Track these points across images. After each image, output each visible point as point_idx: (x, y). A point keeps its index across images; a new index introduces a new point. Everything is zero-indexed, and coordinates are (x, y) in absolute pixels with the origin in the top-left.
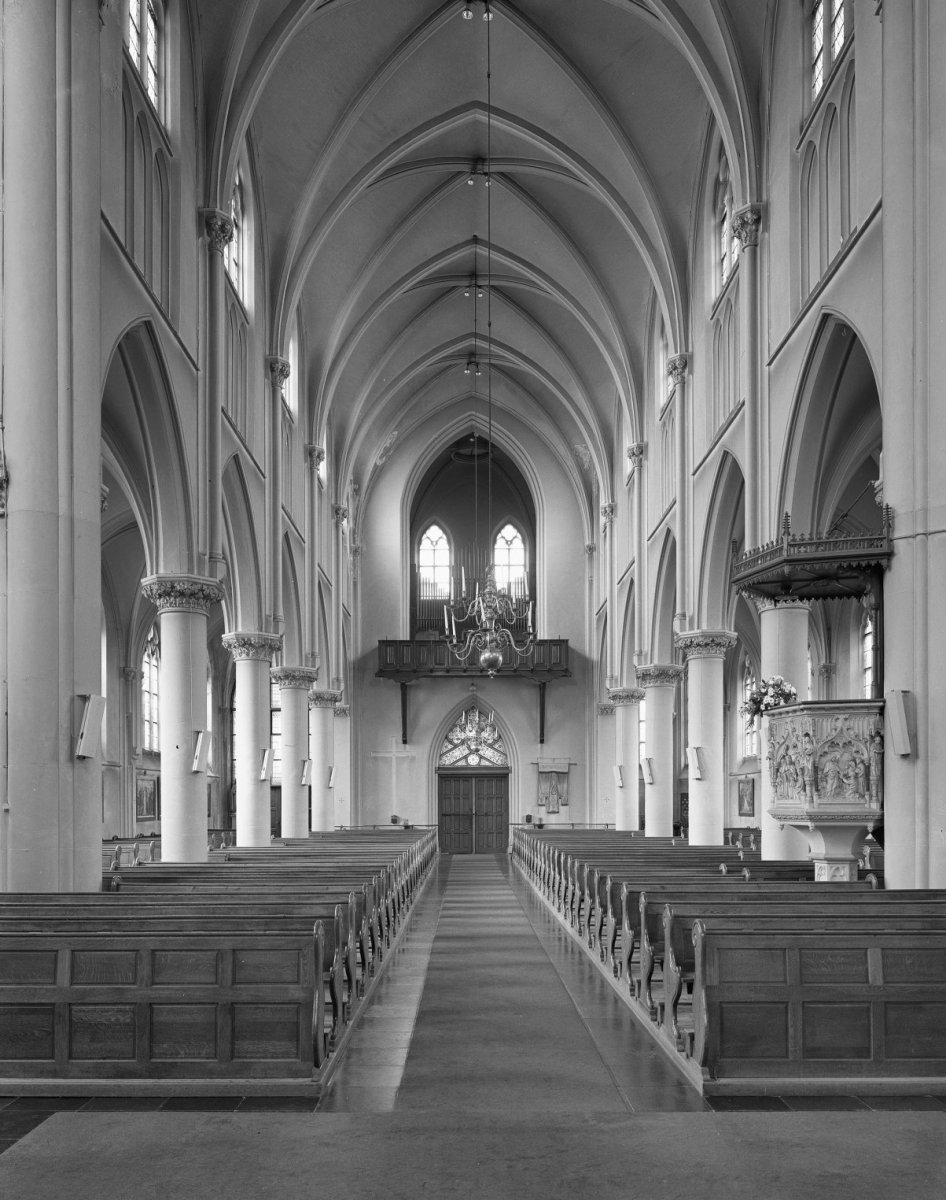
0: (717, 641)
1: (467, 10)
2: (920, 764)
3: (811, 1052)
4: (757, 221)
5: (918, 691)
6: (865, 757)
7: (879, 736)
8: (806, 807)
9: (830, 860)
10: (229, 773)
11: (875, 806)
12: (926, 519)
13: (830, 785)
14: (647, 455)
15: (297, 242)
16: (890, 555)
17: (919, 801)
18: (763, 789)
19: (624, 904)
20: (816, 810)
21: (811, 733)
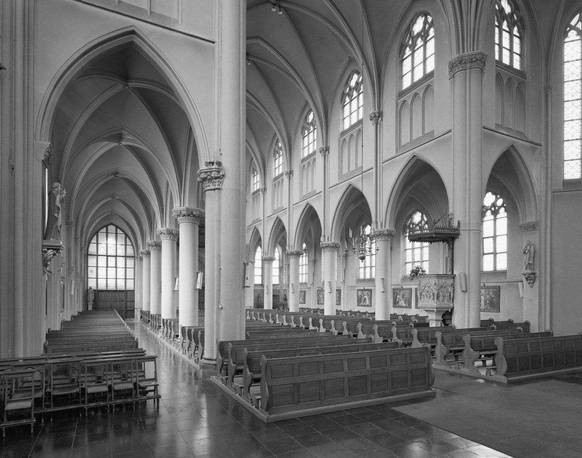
0: (337, 246)
1: (273, 8)
2: (467, 293)
3: (521, 369)
4: (379, 117)
5: (467, 273)
6: (450, 290)
7: (453, 285)
8: (435, 305)
9: (436, 320)
10: (86, 284)
11: (452, 305)
12: (469, 225)
13: (441, 299)
14: (293, 174)
15: (527, 181)
16: (459, 234)
17: (467, 303)
18: (377, 295)
19: (192, 336)
20: (438, 306)
21: (437, 283)
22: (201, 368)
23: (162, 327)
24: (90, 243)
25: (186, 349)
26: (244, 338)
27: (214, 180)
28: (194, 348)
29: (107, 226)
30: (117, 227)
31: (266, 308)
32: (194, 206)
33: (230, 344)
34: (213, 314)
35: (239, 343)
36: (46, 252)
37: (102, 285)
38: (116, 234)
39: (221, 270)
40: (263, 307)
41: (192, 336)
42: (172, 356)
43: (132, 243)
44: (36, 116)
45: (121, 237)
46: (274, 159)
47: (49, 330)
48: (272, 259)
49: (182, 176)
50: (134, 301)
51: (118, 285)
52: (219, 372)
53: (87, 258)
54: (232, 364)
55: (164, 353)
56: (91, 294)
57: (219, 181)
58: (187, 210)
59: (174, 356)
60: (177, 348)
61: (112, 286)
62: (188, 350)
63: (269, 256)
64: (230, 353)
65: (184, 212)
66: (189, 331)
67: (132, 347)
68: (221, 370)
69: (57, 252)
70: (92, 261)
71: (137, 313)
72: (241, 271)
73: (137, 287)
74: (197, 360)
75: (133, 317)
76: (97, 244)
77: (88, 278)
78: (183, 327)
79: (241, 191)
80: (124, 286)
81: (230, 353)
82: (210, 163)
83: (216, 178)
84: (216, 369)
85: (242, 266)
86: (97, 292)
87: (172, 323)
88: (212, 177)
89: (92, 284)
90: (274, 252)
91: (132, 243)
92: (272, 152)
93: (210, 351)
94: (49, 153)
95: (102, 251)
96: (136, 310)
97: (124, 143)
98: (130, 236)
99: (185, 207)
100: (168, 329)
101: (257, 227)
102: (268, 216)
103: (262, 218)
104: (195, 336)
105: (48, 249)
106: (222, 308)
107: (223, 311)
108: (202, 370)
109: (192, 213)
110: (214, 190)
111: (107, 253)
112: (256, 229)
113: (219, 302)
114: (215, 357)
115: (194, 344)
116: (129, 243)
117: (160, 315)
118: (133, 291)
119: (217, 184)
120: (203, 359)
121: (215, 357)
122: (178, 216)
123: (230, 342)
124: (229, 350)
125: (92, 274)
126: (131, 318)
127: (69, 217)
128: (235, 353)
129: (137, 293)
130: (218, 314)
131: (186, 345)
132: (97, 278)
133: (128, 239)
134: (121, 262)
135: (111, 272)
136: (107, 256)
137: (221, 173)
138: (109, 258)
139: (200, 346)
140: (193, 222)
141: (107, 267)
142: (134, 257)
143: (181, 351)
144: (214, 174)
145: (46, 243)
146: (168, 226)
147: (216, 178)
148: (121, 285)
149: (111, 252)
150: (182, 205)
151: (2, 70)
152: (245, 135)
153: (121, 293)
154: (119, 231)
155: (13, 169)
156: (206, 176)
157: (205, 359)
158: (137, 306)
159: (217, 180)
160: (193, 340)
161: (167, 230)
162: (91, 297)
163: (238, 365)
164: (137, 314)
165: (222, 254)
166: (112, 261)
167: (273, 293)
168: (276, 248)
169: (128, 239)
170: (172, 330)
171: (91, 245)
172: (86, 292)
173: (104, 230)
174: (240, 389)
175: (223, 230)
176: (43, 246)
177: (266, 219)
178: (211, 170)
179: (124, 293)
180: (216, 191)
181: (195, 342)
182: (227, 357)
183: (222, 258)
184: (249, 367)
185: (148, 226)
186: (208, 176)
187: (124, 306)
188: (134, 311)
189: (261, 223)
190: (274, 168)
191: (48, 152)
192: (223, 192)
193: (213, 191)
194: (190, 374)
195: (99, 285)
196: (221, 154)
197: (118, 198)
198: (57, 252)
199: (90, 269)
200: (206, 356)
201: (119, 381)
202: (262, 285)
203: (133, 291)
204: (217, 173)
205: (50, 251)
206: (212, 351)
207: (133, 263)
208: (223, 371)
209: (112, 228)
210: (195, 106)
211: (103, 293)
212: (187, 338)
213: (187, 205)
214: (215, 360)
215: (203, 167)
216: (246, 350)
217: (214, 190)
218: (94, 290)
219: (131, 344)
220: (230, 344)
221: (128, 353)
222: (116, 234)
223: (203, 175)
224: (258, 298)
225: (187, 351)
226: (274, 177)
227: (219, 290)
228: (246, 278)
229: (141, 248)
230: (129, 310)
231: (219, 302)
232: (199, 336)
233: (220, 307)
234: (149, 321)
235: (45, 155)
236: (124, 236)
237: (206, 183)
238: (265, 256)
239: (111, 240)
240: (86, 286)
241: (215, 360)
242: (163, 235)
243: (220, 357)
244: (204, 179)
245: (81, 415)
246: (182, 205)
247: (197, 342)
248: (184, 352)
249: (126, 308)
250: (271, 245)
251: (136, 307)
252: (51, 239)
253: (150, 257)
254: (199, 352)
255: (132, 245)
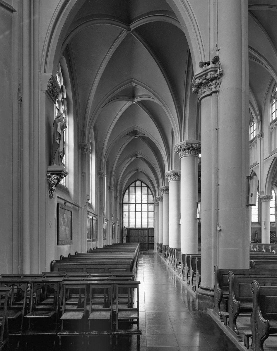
19: (190, 262)
22: (197, 299)
23: (170, 255)
24: (124, 195)
25: (186, 276)
26: (248, 267)
27: (211, 83)
28: (192, 275)
29: (135, 182)
30: (142, 182)
31: (263, 242)
32: (193, 140)
33: (231, 273)
34: (210, 237)
35: (242, 272)
36: (50, 177)
37: (132, 225)
38: (141, 187)
39: (219, 186)
40: (261, 242)
41: (190, 262)
42: (176, 281)
43: (152, 193)
44: (41, 51)
45: (145, 188)
46: (271, 105)
47: (76, 252)
48: (269, 198)
49: (182, 113)
50: (154, 237)
51: (143, 225)
52: (217, 306)
53: (123, 206)
54: (235, 301)
55: (170, 278)
56: (125, 231)
57: (216, 83)
58: (187, 143)
59: (177, 281)
60: (178, 274)
61: (138, 226)
62: (187, 277)
63: (266, 194)
64: (231, 284)
65: (184, 147)
66: (188, 257)
67: (126, 270)
68: (219, 304)
69: (60, 176)
70: (125, 208)
71: (156, 246)
72: (245, 186)
73: (156, 226)
74: (194, 287)
75: (154, 249)
76: (129, 195)
77: (123, 220)
78: (183, 254)
79: (243, 90)
80: (147, 225)
81: (231, 284)
82: (205, 63)
83: (212, 80)
84: (213, 301)
85: (245, 180)
86: (129, 230)
87: (176, 251)
88: (208, 80)
89: (126, 224)
90: (271, 193)
91: (152, 193)
92: (269, 97)
93: (207, 279)
94: (53, 84)
95: (132, 200)
96: (155, 243)
97: (136, 100)
98: (151, 188)
99: (185, 141)
100: (173, 257)
101: (254, 171)
102: (265, 158)
103: (259, 162)
104: (193, 263)
105: (52, 174)
106: (220, 230)
107: (222, 234)
108: (197, 301)
109: (192, 146)
110: (210, 95)
111: (135, 202)
112: (253, 172)
113: (217, 223)
114: (212, 287)
115: (191, 271)
116: (150, 193)
117: (168, 246)
118: (153, 229)
119: (214, 86)
120: (200, 288)
121: (212, 287)
122: (179, 151)
123: (231, 270)
124: (230, 280)
125: (125, 218)
126: (151, 249)
127: (100, 169)
128: (237, 286)
129: (156, 231)
130: (217, 237)
131: (186, 272)
132: (129, 220)
133: (149, 191)
134: (145, 206)
135: (138, 215)
136: (136, 204)
137: (218, 71)
138: (136, 205)
139: (197, 272)
140: (190, 155)
141: (136, 211)
142: (154, 203)
143: (181, 278)
144: (210, 75)
145: (51, 168)
146: (174, 169)
147: (212, 80)
148: (145, 225)
149: (139, 201)
150: (182, 140)
151: (14, 12)
152: (247, 41)
153: (145, 231)
154: (143, 185)
155: (21, 100)
156: (201, 81)
157: (202, 288)
158: (156, 240)
159: (214, 82)
160: (191, 267)
161: (173, 172)
162: (125, 234)
163: (242, 301)
164: (156, 246)
165: (220, 168)
166: (138, 206)
167: (270, 230)
168: (273, 190)
169: (149, 191)
170: (176, 257)
171: (125, 196)
172: (122, 229)
173: (133, 185)
174: (246, 338)
175: (221, 139)
176: (48, 171)
177: (263, 161)
178: (207, 72)
179: (147, 231)
180: (213, 95)
181: (193, 269)
182: (227, 289)
183: (221, 172)
184: (261, 309)
185: (161, 176)
186: (204, 80)
187: (147, 241)
188: (154, 244)
189: (258, 166)
190: (271, 113)
191: (51, 82)
192: (221, 94)
193: (209, 97)
194: (189, 302)
195: (130, 225)
196: (218, 50)
197: (141, 156)
198: (60, 176)
199: (124, 213)
200: (202, 285)
201: (101, 307)
202: (259, 223)
203: (153, 229)
204: (213, 73)
205: (53, 176)
206: (209, 280)
207: (153, 208)
208: (222, 305)
209: (138, 183)
210: (190, 11)
211: (133, 231)
212: (186, 264)
213: (187, 139)
214: (213, 291)
215: (198, 70)
216: (256, 283)
217: (210, 95)
218: (127, 229)
219: (126, 267)
220: (231, 273)
221: (116, 276)
222: (141, 187)
223: (198, 81)
224: (255, 234)
225: (186, 277)
226: (271, 121)
227: (217, 210)
228: (250, 194)
229: (157, 195)
230: (150, 243)
231: (217, 223)
232: (196, 263)
233: (218, 228)
234: (168, 255)
235: (49, 86)
236: (146, 188)
237: (202, 90)
238: (262, 195)
239: (138, 192)
240: (122, 226)
241: (213, 291)
242: (169, 177)
243: (218, 288)
244: (200, 85)
245: (54, 343)
246: (182, 140)
247: (194, 269)
248: (184, 278)
249: (148, 242)
250: (269, 185)
251: (155, 241)
252: (54, 164)
253: (162, 202)
254: (196, 279)
255: (153, 195)
